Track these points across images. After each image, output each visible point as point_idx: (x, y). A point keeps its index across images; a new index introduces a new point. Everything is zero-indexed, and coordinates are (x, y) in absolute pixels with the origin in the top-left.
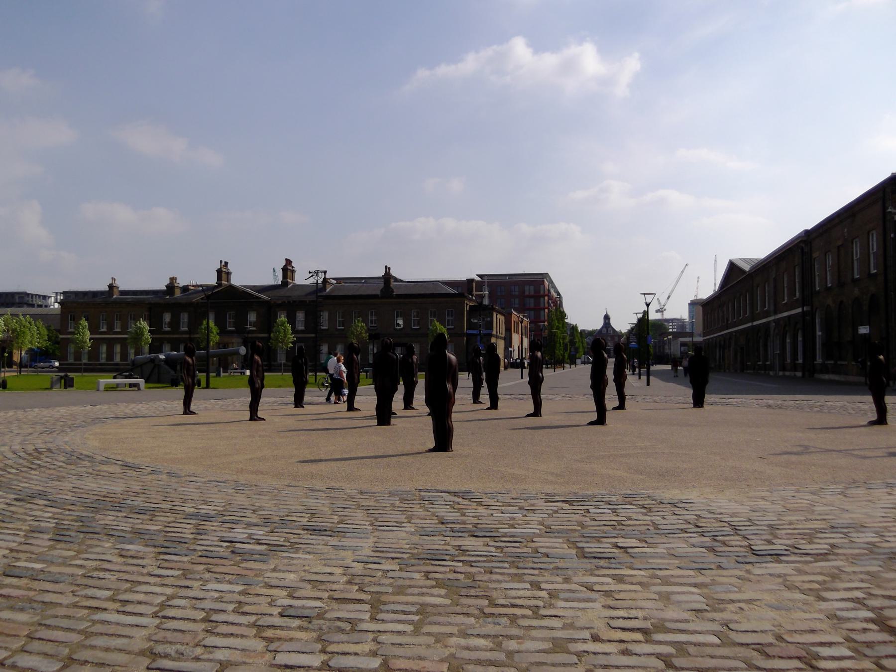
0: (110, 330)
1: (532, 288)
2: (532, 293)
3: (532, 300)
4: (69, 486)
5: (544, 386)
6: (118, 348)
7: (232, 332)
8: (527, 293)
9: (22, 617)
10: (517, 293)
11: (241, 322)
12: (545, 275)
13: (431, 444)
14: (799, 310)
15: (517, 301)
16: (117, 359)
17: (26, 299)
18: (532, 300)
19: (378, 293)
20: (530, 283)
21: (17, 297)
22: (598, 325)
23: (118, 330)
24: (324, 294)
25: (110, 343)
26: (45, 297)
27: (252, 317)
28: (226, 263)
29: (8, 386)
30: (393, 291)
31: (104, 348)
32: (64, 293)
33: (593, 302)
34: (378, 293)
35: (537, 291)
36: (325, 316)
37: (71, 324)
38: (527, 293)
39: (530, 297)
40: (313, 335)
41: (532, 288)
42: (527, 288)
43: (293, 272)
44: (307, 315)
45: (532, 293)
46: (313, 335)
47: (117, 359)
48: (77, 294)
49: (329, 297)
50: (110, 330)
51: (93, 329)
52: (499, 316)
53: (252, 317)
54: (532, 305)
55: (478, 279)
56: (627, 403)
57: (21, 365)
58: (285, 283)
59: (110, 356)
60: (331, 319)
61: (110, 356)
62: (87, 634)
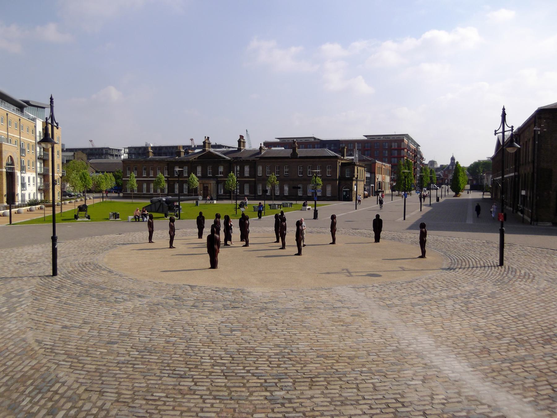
0: (148, 176)
1: (396, 144)
2: (396, 147)
3: (396, 152)
4: (89, 279)
5: (286, 237)
6: (152, 186)
7: (210, 177)
8: (393, 147)
9: (65, 312)
10: (387, 147)
11: (215, 171)
12: (407, 136)
13: (210, 266)
14: (513, 174)
15: (387, 152)
16: (152, 191)
17: (109, 151)
18: (396, 152)
19: (289, 155)
20: (395, 141)
21: (104, 151)
22: (448, 162)
23: (152, 176)
24: (260, 156)
25: (148, 183)
26: (119, 150)
27: (221, 169)
28: (208, 138)
29: (91, 218)
30: (297, 155)
31: (145, 186)
32: (129, 148)
33: (436, 152)
34: (289, 155)
35: (399, 146)
36: (260, 169)
37: (128, 172)
38: (393, 147)
39: (395, 149)
40: (254, 179)
41: (396, 144)
42: (393, 144)
43: (244, 142)
44: (250, 168)
45: (396, 147)
46: (254, 179)
47: (152, 191)
48: (135, 148)
49: (262, 158)
50: (148, 176)
51: (139, 175)
52: (359, 168)
53: (221, 169)
54: (396, 155)
55: (366, 138)
56: (303, 249)
57: (107, 192)
58: (239, 149)
59: (148, 189)
60: (264, 171)
61: (148, 189)
62: (75, 315)
